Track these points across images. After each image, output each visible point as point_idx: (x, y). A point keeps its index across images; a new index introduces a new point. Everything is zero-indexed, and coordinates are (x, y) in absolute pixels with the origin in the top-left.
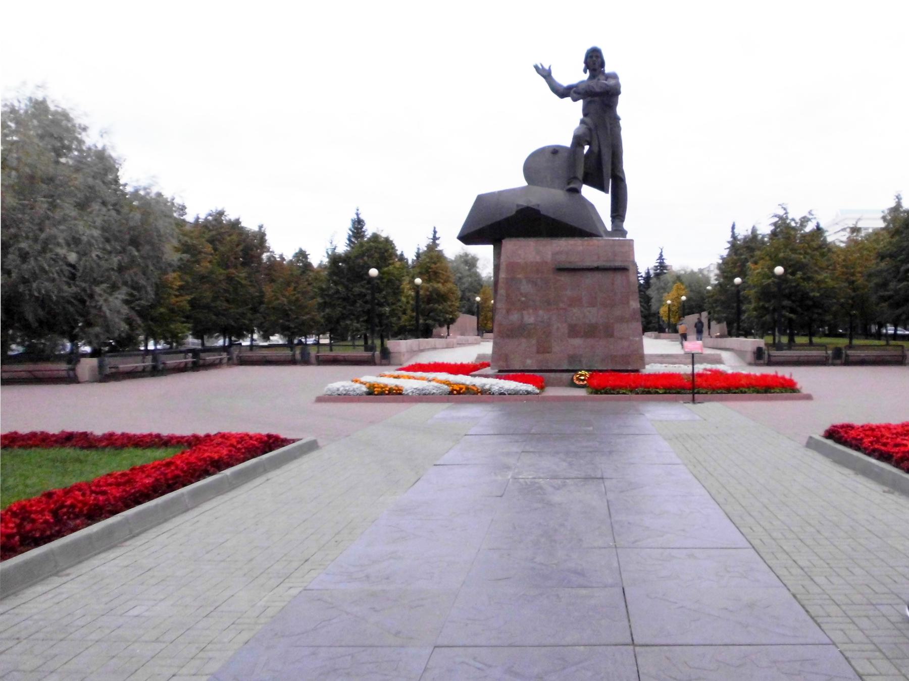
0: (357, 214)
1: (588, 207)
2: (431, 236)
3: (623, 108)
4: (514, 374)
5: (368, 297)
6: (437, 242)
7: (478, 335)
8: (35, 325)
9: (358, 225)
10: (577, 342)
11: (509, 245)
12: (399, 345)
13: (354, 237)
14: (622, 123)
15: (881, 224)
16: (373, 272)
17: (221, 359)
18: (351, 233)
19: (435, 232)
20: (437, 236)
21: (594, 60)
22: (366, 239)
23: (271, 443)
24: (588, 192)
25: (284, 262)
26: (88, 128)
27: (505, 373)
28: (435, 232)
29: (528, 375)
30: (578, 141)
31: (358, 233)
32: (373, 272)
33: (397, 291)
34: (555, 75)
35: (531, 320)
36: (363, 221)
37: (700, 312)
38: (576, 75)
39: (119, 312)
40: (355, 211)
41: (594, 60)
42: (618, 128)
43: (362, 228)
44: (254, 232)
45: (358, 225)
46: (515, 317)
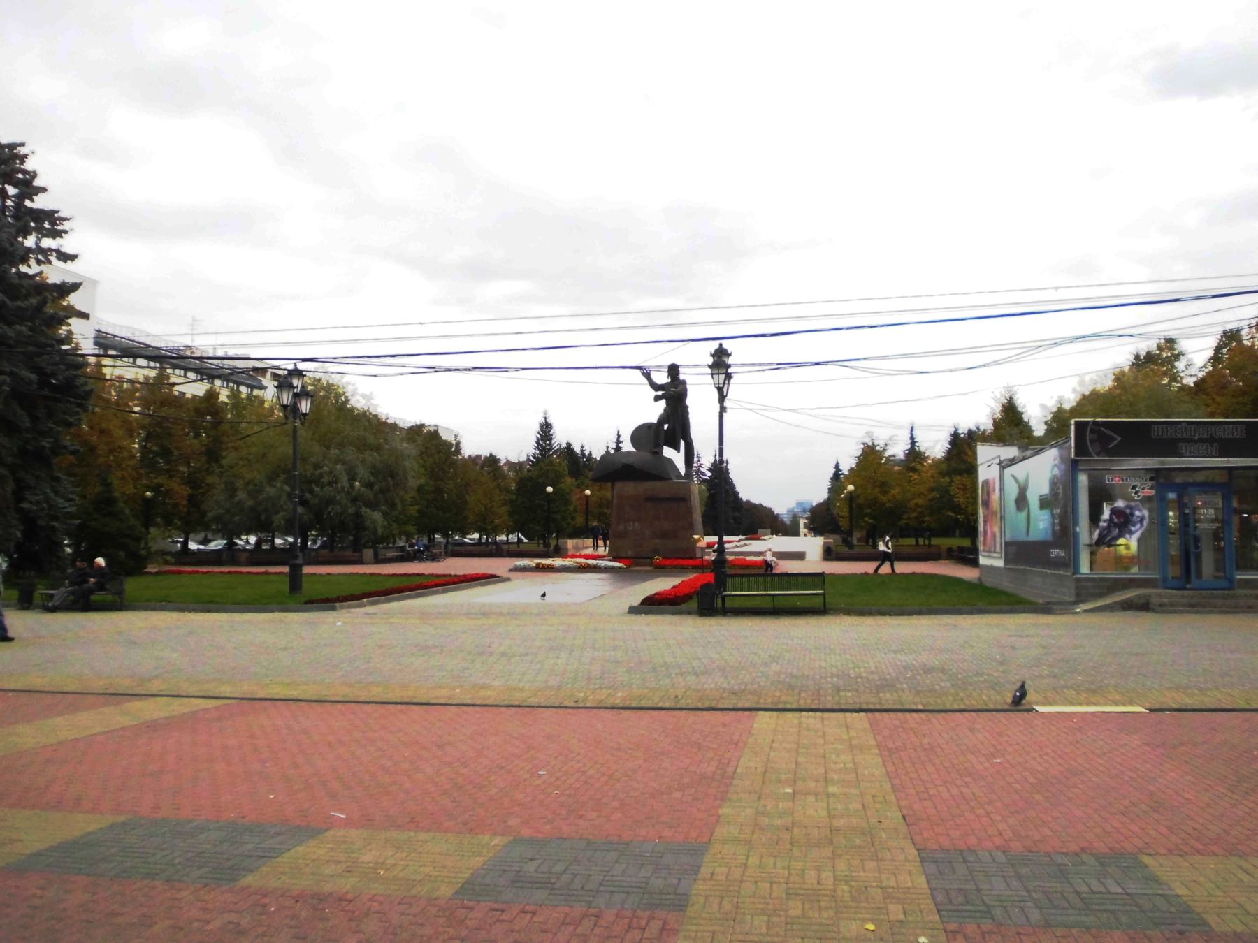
0: (545, 418)
2: (615, 440)
4: (733, 593)
5: (546, 508)
6: (621, 445)
9: (546, 430)
10: (657, 541)
11: (619, 485)
12: (567, 542)
13: (542, 440)
14: (689, 409)
15: (943, 455)
16: (549, 489)
17: (441, 552)
18: (539, 436)
19: (619, 436)
20: (621, 439)
23: (494, 576)
24: (668, 452)
27: (615, 559)
28: (619, 436)
29: (1131, 703)
31: (546, 436)
32: (549, 489)
33: (567, 502)
35: (631, 528)
36: (550, 425)
38: (662, 378)
40: (543, 415)
41: (673, 370)
42: (687, 413)
43: (550, 431)
45: (546, 430)
46: (621, 527)
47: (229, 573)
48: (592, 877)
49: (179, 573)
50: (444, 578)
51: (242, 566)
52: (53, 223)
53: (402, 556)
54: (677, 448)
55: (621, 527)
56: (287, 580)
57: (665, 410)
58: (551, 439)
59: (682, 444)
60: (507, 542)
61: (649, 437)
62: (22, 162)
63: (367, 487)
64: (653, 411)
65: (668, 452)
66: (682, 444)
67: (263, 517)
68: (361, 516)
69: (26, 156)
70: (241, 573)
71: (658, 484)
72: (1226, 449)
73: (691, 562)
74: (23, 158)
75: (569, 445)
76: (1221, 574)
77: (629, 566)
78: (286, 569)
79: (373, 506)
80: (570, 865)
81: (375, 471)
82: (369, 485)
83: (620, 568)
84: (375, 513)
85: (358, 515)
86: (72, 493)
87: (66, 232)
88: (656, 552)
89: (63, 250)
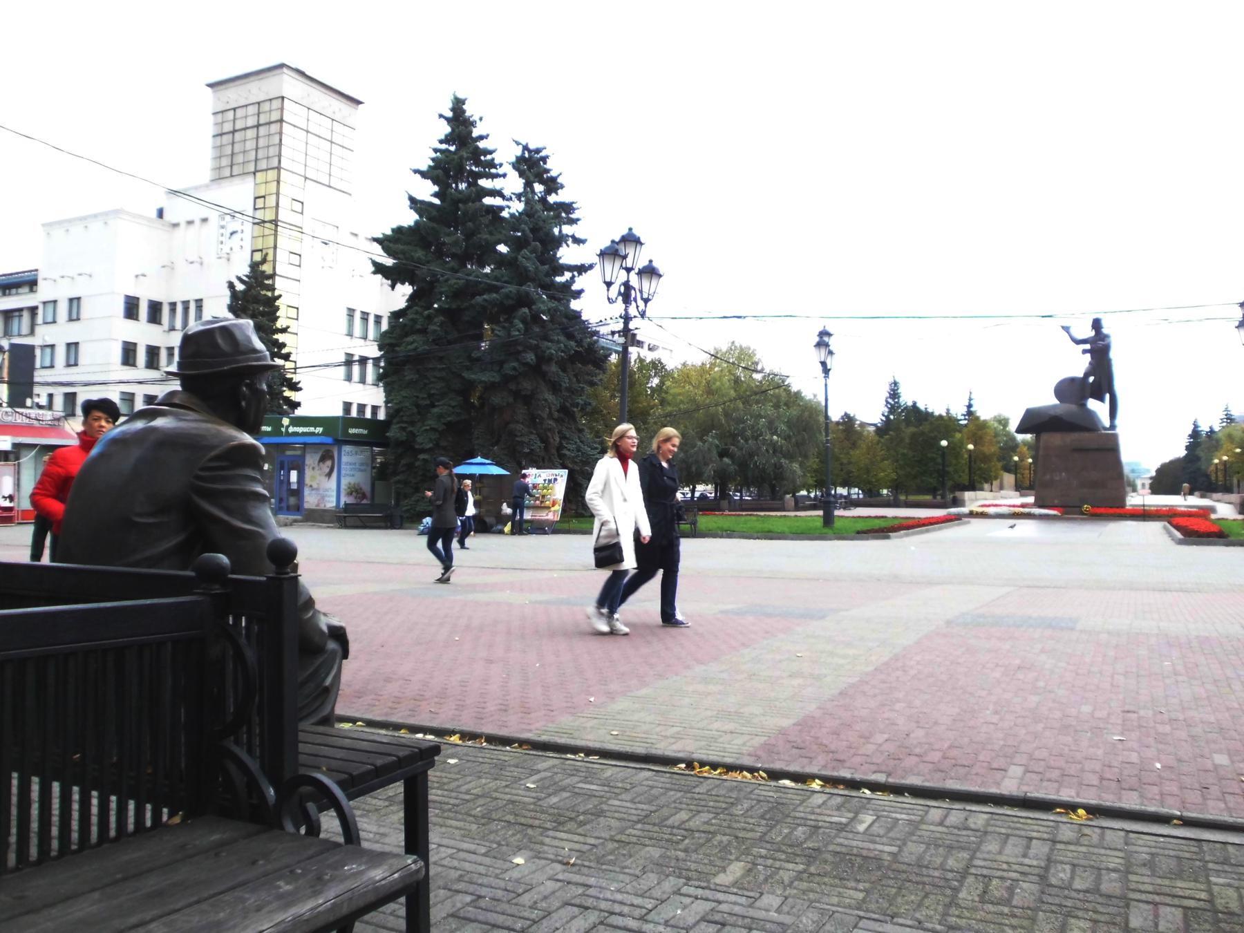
0: (446, 560)
1: (1091, 415)
3: (1113, 354)
7: (1016, 491)
8: (766, 486)
11: (1045, 437)
13: (890, 398)
21: (1097, 324)
22: (428, 521)
24: (1092, 404)
25: (856, 453)
26: (815, 346)
30: (1087, 375)
32: (944, 443)
34: (1073, 331)
35: (1057, 478)
37: (679, 448)
39: (757, 402)
41: (1097, 324)
43: (897, 389)
44: (1092, 358)
47: (781, 516)
48: (821, 831)
49: (739, 515)
50: (877, 521)
51: (789, 511)
52: (568, 213)
53: (815, 504)
54: (1102, 399)
55: (1048, 477)
56: (822, 520)
57: (1090, 363)
58: (899, 397)
59: (1107, 396)
60: (808, 497)
61: (1072, 390)
62: (545, 163)
63: (785, 440)
64: (1078, 364)
65: (1092, 404)
66: (1107, 396)
67: (694, 469)
68: (781, 466)
69: (547, 157)
70: (760, 516)
71: (1086, 435)
72: (239, 475)
73: (1118, 511)
74: (544, 159)
75: (915, 403)
76: (630, 562)
77: (1063, 513)
78: (821, 513)
79: (790, 457)
80: (726, 809)
81: (789, 423)
82: (787, 438)
83: (1055, 515)
84: (794, 465)
85: (778, 466)
86: (595, 442)
87: (578, 220)
88: (1084, 501)
89: (577, 236)
